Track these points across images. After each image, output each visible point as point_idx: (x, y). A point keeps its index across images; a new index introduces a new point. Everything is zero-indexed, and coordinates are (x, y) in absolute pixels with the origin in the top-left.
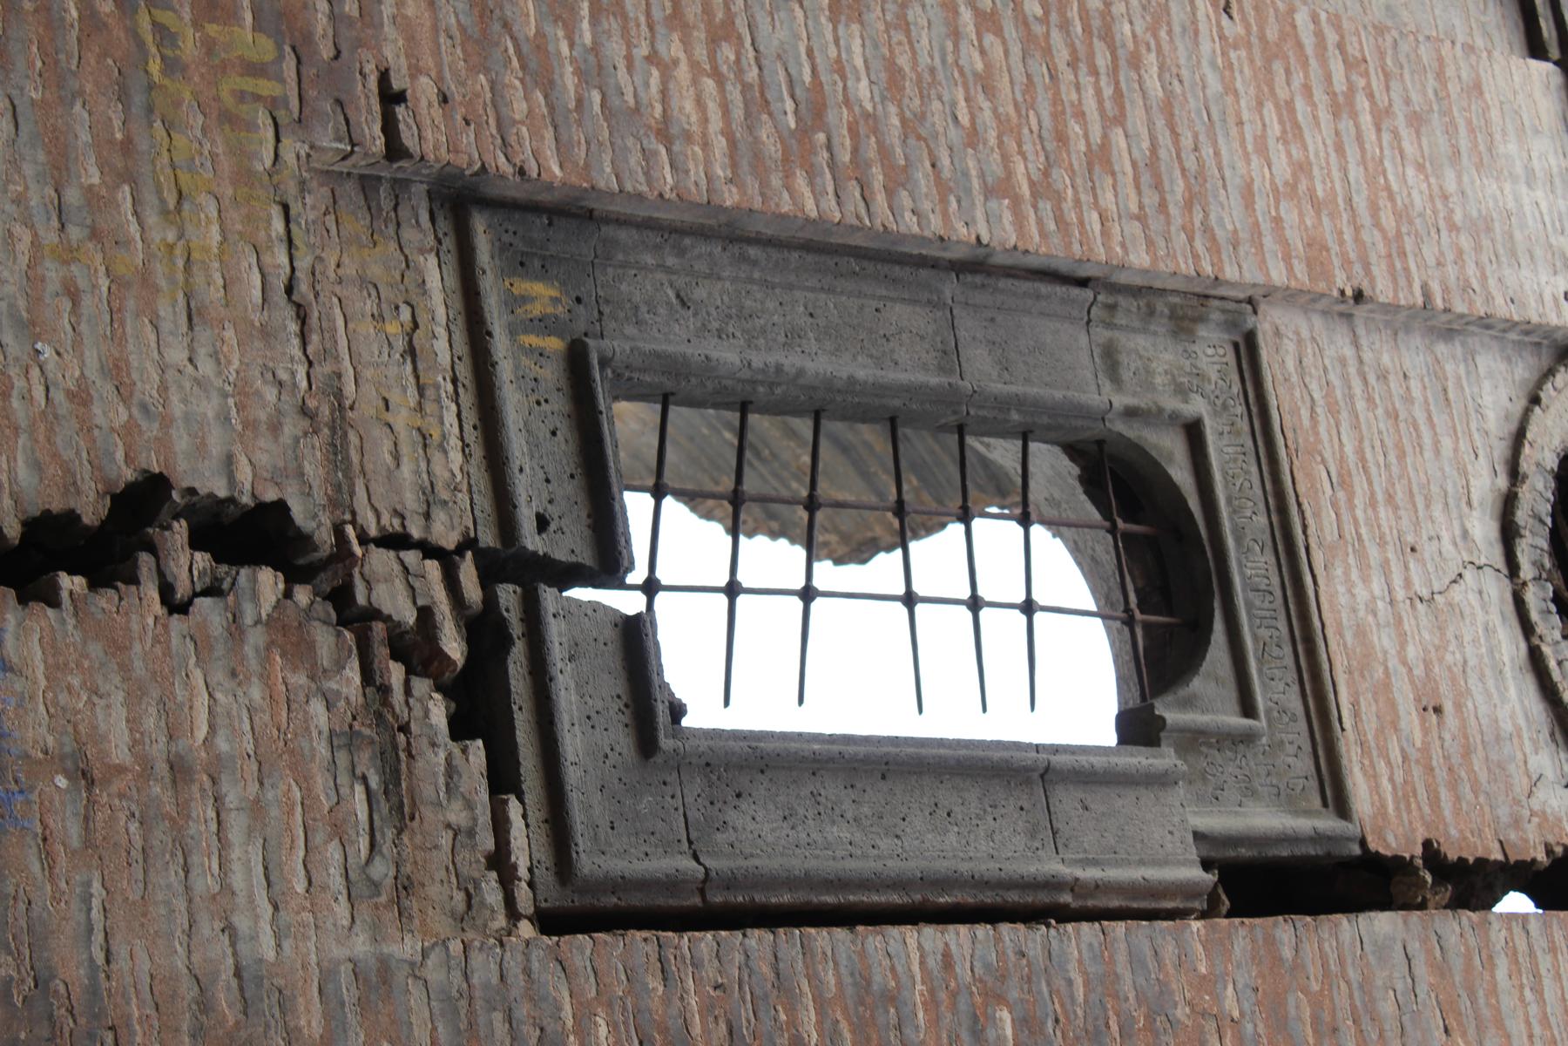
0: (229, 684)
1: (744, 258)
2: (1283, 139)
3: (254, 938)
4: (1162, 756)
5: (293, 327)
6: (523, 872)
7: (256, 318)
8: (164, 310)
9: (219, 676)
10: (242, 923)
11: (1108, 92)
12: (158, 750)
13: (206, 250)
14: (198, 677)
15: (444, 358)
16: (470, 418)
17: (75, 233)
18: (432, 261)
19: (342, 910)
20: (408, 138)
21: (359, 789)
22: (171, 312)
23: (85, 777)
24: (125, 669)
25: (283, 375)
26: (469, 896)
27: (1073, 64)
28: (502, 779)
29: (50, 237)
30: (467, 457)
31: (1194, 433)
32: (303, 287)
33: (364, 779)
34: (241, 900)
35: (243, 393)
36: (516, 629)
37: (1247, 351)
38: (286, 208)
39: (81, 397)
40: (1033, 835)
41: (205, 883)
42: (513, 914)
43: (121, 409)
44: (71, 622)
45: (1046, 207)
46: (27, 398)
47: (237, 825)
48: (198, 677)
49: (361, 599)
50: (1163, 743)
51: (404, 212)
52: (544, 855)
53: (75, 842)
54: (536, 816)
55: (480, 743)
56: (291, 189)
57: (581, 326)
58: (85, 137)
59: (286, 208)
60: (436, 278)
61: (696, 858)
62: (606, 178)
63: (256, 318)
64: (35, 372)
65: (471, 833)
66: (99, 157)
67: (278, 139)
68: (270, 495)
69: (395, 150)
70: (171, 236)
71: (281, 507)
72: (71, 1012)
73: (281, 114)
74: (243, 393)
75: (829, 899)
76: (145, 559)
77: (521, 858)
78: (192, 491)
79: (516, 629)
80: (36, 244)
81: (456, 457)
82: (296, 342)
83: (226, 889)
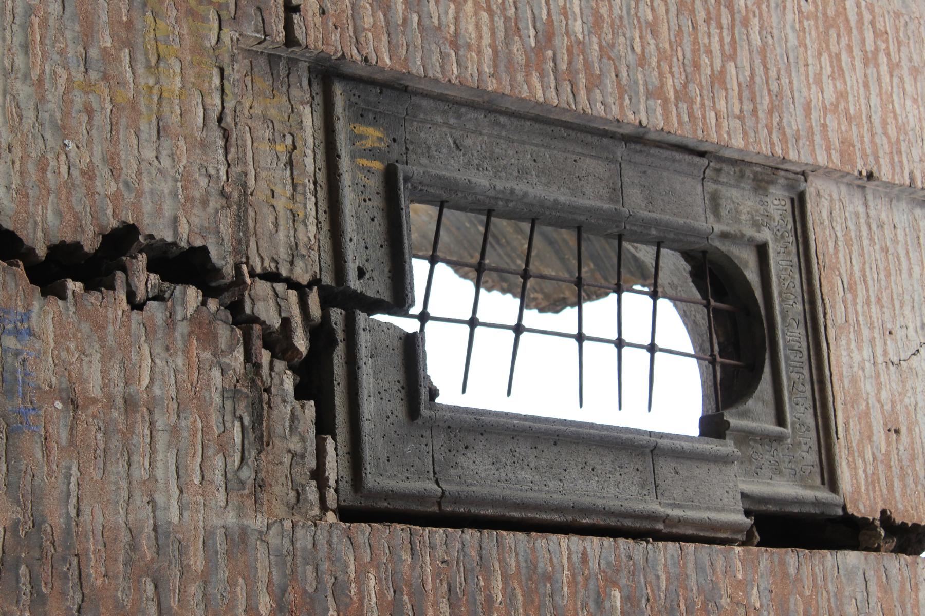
0: (164, 355)
1: (497, 123)
2: (832, 77)
3: (167, 508)
4: (726, 445)
5: (221, 143)
6: (332, 482)
7: (198, 135)
8: (143, 126)
9: (158, 349)
10: (160, 498)
11: (727, 39)
12: (118, 391)
13: (172, 92)
14: (145, 349)
15: (310, 169)
16: (323, 206)
17: (93, 75)
18: (308, 109)
19: (221, 496)
20: (299, 34)
21: (237, 424)
22: (147, 128)
23: (73, 403)
24: (102, 340)
25: (212, 171)
26: (298, 494)
27: (707, 21)
28: (324, 425)
29: (79, 77)
30: (319, 229)
31: (762, 251)
32: (229, 119)
33: (241, 419)
34: (161, 485)
35: (187, 180)
36: (340, 335)
37: (799, 204)
38: (222, 71)
39: (89, 174)
40: (643, 486)
41: (140, 472)
42: (324, 507)
43: (113, 184)
44: (72, 309)
45: (683, 106)
46: (57, 172)
47: (162, 440)
48: (145, 349)
49: (248, 310)
50: (727, 437)
51: (293, 79)
52: (346, 474)
53: (64, 442)
54: (342, 449)
55: (312, 402)
56: (226, 59)
57: (395, 156)
58: (104, 18)
59: (222, 71)
60: (309, 120)
61: (437, 483)
62: (417, 68)
63: (198, 135)
64: (63, 157)
65: (303, 457)
66: (112, 30)
67: (220, 29)
68: (198, 243)
69: (291, 40)
70: (151, 82)
71: (204, 250)
72: (53, 543)
73: (224, 14)
74: (187, 180)
75: (516, 515)
76: (120, 275)
77: (331, 475)
78: (151, 237)
79: (340, 335)
80: (69, 80)
81: (312, 229)
82: (221, 151)
83: (152, 478)
